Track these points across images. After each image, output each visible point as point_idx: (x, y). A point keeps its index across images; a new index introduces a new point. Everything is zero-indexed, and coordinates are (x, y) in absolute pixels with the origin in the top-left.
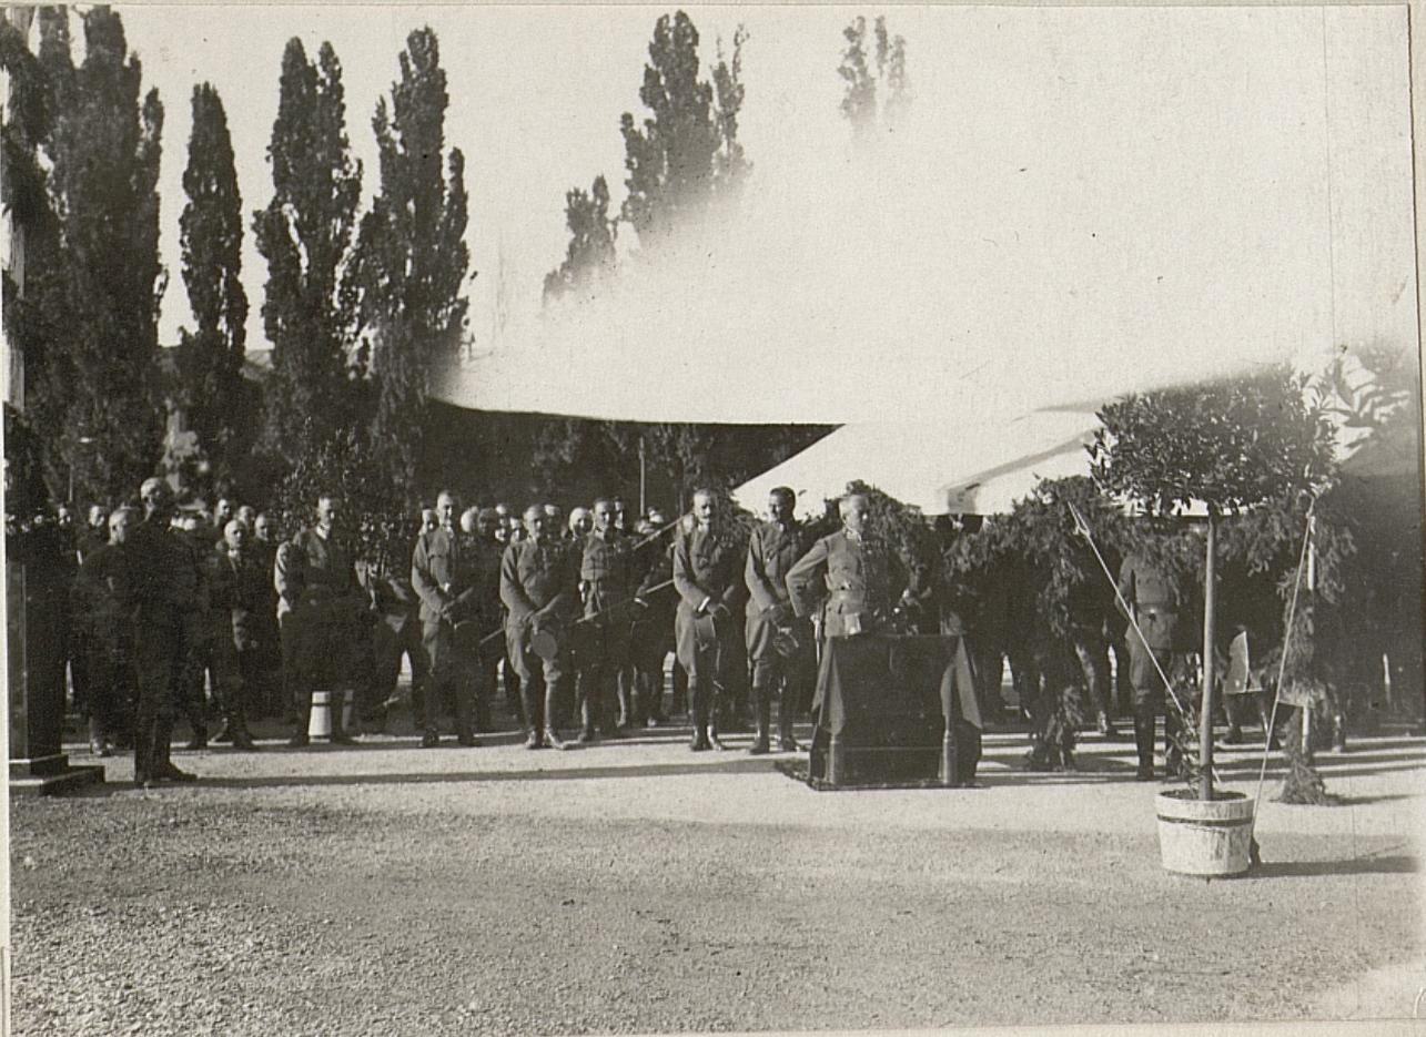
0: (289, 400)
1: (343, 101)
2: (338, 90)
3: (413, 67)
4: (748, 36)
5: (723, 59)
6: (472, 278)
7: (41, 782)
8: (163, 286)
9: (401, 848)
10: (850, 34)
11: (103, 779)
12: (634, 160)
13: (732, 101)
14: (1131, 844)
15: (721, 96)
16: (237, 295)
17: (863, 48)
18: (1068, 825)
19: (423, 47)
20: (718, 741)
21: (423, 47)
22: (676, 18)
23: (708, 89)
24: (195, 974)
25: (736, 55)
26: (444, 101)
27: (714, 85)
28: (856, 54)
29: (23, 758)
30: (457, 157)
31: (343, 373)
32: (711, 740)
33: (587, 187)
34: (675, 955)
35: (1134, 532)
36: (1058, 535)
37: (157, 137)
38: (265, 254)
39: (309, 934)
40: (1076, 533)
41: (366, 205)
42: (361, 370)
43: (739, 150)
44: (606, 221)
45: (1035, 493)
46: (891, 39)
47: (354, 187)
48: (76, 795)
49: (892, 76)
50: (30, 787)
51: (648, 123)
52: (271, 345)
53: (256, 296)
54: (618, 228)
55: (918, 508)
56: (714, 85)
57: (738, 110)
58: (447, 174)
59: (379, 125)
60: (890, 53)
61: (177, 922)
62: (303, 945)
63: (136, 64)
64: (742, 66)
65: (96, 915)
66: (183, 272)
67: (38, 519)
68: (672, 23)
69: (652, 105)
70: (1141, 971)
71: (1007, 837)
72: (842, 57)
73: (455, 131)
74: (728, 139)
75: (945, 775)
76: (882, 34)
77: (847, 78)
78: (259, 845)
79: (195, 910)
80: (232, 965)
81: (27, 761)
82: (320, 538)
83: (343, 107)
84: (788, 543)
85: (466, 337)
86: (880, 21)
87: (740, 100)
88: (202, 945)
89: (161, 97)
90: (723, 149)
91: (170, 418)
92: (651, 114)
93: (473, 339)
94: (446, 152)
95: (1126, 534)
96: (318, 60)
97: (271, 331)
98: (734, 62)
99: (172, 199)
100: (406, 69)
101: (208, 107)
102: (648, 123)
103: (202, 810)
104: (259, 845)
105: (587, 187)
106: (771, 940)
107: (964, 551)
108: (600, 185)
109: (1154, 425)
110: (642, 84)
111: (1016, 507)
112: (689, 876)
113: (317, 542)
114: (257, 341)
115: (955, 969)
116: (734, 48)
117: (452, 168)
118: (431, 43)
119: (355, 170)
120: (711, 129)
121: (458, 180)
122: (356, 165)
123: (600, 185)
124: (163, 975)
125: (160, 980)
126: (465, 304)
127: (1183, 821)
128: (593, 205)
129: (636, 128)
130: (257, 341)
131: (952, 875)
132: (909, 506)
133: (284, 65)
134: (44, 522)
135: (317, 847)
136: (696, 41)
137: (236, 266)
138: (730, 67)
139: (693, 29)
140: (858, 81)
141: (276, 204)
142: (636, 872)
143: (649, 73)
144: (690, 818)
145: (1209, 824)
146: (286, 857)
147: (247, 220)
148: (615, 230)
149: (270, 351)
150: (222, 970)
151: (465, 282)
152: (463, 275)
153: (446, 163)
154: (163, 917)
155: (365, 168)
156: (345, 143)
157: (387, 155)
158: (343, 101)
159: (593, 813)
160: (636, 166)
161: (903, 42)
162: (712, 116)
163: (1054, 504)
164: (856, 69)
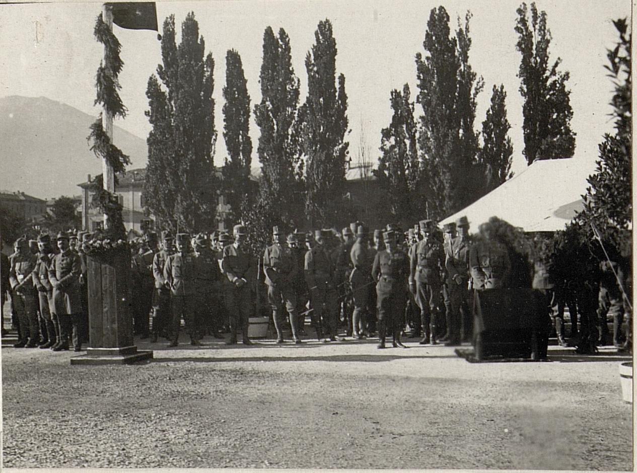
0: (270, 189)
1: (290, 54)
2: (288, 49)
3: (321, 37)
4: (472, 15)
5: (461, 27)
6: (349, 132)
7: (123, 358)
8: (215, 140)
9: (270, 388)
10: (520, 11)
11: (152, 357)
12: (421, 75)
13: (466, 44)
14: (613, 388)
15: (460, 44)
16: (248, 142)
17: (526, 18)
18: (584, 379)
19: (325, 30)
21: (325, 30)
22: (439, 9)
23: (455, 40)
24: (155, 444)
25: (467, 24)
26: (335, 52)
27: (457, 39)
28: (523, 21)
29: (116, 347)
30: (342, 78)
31: (293, 176)
33: (401, 89)
34: (375, 439)
35: (622, 238)
36: (586, 240)
37: (212, 75)
38: (259, 125)
39: (213, 427)
40: (594, 238)
41: (302, 100)
42: (300, 175)
43: (470, 67)
44: (409, 104)
45: (575, 219)
46: (539, 13)
47: (297, 92)
48: (138, 364)
49: (540, 30)
51: (428, 58)
52: (262, 165)
53: (255, 144)
55: (522, 228)
56: (457, 39)
57: (468, 50)
58: (337, 85)
59: (308, 64)
60: (539, 20)
61: (158, 421)
62: (208, 432)
63: (203, 41)
64: (470, 30)
65: (124, 417)
66: (223, 133)
67: (120, 241)
68: (437, 12)
69: (430, 50)
70: (596, 450)
71: (554, 385)
72: (516, 22)
73: (341, 66)
74: (464, 63)
75: (532, 357)
76: (534, 10)
77: (519, 32)
78: (208, 387)
79: (167, 415)
80: (173, 440)
81: (118, 349)
82: (234, 248)
83: (290, 57)
84: (464, 246)
85: (347, 159)
86: (533, 5)
87: (469, 46)
88: (164, 431)
89: (213, 57)
90: (462, 67)
91: (220, 198)
92: (429, 54)
93: (351, 160)
94: (337, 75)
95: (618, 239)
96: (278, 36)
97: (262, 159)
98: (466, 28)
99: (219, 100)
100: (318, 40)
101: (234, 59)
102: (428, 58)
103: (189, 370)
104: (208, 387)
105: (401, 89)
106: (422, 432)
107: (543, 249)
108: (406, 88)
109: (613, 184)
110: (424, 40)
111: (567, 227)
112: (396, 402)
113: (233, 250)
114: (256, 165)
115: (505, 447)
116: (466, 21)
117: (340, 83)
118: (329, 27)
119: (296, 85)
120: (456, 59)
121: (342, 88)
122: (297, 82)
123: (406, 88)
124: (141, 445)
125: (138, 447)
126: (347, 144)
130: (256, 165)
131: (523, 402)
133: (265, 40)
134: (122, 242)
135: (232, 388)
136: (448, 19)
137: (247, 130)
138: (464, 30)
139: (447, 14)
140: (524, 33)
141: (263, 102)
142: (372, 400)
143: (427, 35)
144: (405, 375)
146: (217, 391)
147: (252, 107)
149: (261, 168)
150: (168, 443)
151: (346, 133)
152: (345, 131)
153: (337, 81)
154: (153, 418)
155: (301, 82)
156: (292, 72)
157: (311, 78)
158: (290, 54)
159: (362, 373)
160: (422, 78)
161: (545, 14)
162: (457, 54)
163: (584, 225)
164: (523, 28)
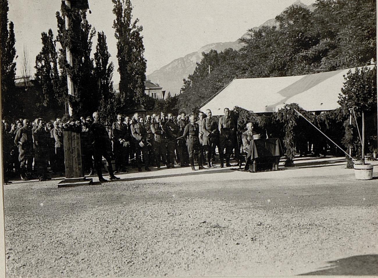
20: (213, 166)
30: (12, 25)
32: (211, 165)
43: (87, 21)
50: (87, 183)
54: (56, 43)
55: (252, 111)
82: (118, 124)
90: (83, 22)
108: (50, 31)
111: (279, 110)
113: (118, 125)
121: (12, 31)
126: (15, 64)
127: (362, 169)
128: (49, 37)
129: (60, 16)
132: (250, 111)
145: (367, 169)
148: (55, 44)
152: (14, 57)
153: (8, 26)
